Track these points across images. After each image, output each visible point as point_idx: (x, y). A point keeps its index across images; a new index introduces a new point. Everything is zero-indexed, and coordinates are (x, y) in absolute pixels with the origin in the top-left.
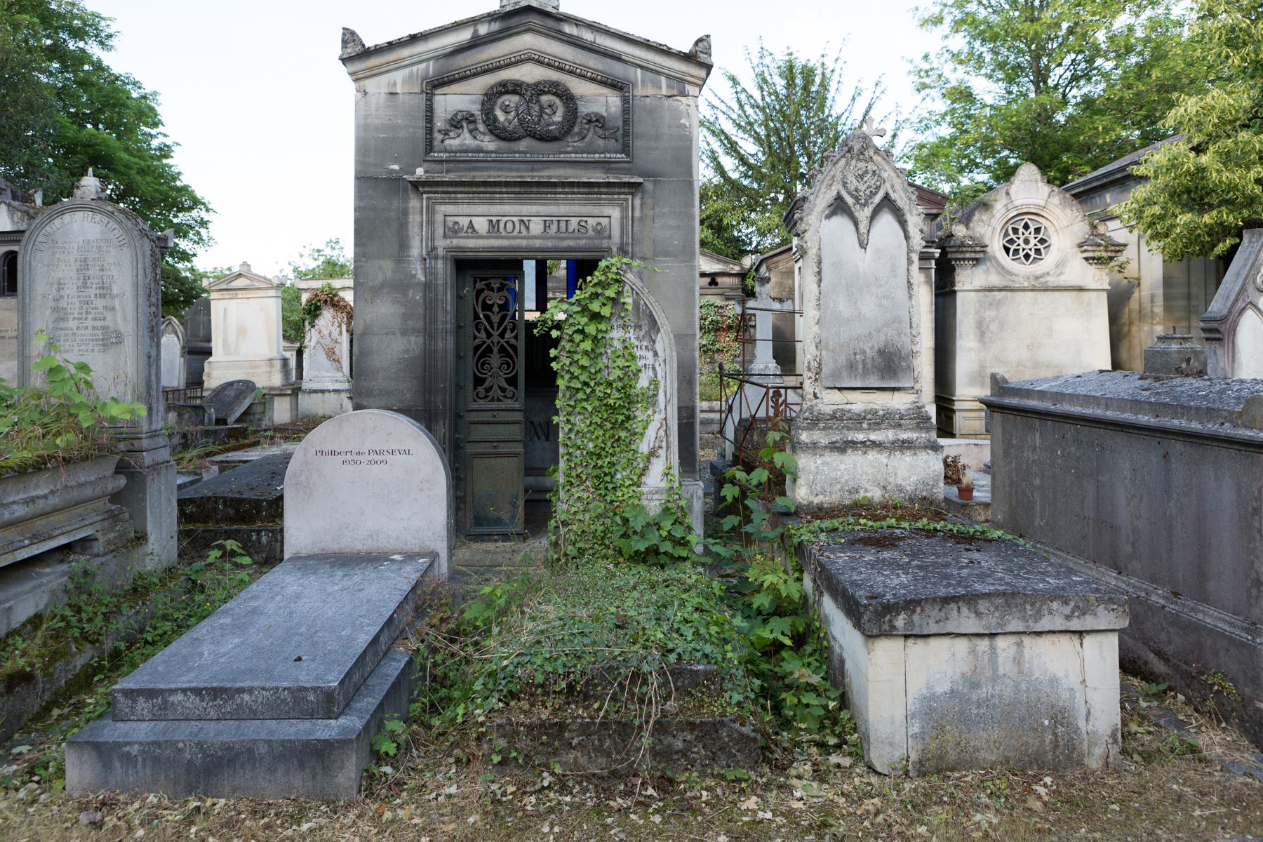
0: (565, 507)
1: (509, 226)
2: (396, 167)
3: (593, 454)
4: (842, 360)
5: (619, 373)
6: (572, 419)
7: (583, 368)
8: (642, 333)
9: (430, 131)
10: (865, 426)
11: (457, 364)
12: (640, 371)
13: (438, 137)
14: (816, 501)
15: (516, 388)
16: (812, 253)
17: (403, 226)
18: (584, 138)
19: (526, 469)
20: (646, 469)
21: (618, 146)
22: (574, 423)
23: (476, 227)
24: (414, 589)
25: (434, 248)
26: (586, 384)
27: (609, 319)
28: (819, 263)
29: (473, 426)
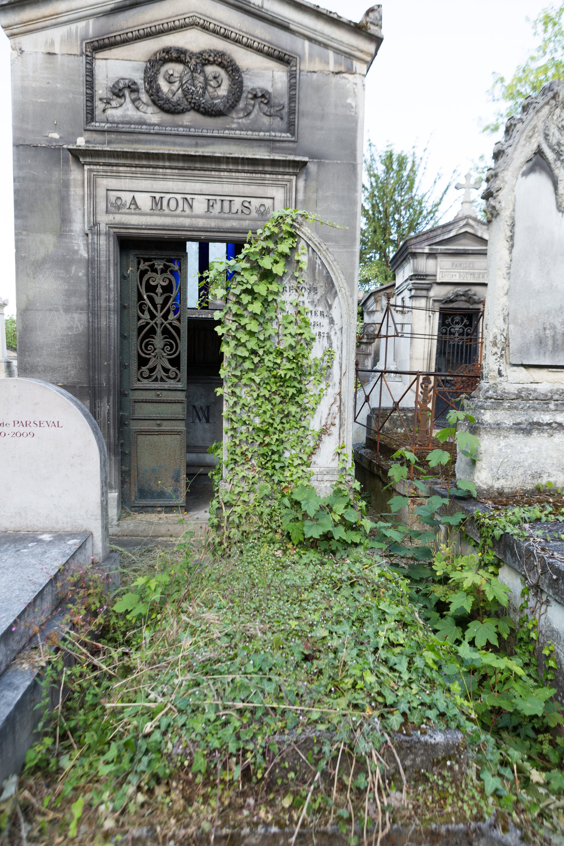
0: (228, 487)
1: (173, 204)
2: (56, 136)
3: (260, 430)
4: (531, 335)
5: (290, 341)
6: (237, 391)
7: (252, 334)
8: (317, 297)
9: (90, 98)
10: (552, 406)
11: (121, 343)
12: (313, 339)
13: (100, 106)
14: (497, 485)
15: (179, 369)
16: (505, 214)
17: (64, 199)
18: (249, 114)
19: (188, 447)
20: (316, 447)
21: (283, 124)
22: (239, 395)
23: (139, 203)
24: (55, 578)
25: (96, 224)
26: (254, 352)
27: (281, 278)
28: (513, 225)
29: (137, 404)
